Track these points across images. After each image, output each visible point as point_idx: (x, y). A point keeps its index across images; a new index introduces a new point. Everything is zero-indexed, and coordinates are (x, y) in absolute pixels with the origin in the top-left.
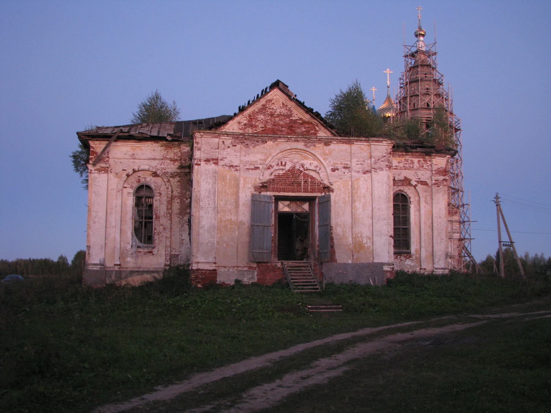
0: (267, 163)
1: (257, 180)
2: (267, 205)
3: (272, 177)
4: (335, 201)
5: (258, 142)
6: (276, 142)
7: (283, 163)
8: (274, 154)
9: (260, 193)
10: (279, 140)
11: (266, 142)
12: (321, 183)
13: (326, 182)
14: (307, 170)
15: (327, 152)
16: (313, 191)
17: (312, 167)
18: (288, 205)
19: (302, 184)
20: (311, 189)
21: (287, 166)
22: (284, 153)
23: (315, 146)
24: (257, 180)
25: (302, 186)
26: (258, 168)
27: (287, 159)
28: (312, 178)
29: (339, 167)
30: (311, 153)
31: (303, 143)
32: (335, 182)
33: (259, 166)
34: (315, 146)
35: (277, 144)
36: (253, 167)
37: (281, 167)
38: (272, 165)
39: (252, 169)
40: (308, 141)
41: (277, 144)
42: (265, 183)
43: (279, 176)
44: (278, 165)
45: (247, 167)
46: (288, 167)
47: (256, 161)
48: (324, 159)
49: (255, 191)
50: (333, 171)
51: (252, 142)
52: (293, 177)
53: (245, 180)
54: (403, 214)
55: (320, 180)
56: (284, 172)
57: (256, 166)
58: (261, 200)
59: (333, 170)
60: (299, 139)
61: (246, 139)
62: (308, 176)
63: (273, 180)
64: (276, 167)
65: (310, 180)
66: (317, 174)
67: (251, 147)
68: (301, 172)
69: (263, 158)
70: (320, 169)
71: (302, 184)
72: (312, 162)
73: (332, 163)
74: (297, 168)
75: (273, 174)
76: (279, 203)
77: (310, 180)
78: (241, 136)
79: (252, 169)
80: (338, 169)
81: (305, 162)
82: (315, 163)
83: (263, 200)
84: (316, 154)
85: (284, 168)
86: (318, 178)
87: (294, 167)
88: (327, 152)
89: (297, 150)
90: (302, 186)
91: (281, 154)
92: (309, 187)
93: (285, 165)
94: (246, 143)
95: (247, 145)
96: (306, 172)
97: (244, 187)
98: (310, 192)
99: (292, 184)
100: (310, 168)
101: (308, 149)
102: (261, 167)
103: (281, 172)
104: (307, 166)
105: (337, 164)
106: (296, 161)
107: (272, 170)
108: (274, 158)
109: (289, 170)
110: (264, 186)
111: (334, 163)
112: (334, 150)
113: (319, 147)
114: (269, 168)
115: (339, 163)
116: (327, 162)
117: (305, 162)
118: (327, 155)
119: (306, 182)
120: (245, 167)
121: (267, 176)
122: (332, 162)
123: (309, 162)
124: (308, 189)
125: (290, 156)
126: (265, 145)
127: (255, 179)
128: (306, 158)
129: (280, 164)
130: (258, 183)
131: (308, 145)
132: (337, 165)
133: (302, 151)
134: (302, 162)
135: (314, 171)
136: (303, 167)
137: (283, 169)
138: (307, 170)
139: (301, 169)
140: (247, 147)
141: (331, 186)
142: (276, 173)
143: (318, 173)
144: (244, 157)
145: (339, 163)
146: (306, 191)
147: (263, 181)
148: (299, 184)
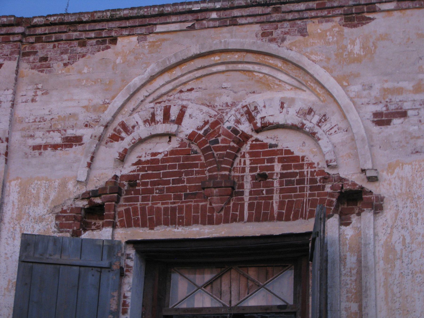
0: (107, 116)
1: (70, 186)
2: (91, 278)
3: (128, 169)
4: (390, 249)
5: (83, 44)
6: (151, 38)
7: (174, 113)
8: (137, 81)
9: (76, 234)
10: (159, 28)
11: (114, 41)
12: (326, 178)
13: (349, 173)
14: (266, 127)
15: (357, 49)
16: (289, 213)
17: (291, 117)
18: (210, 283)
19: (247, 187)
20: (281, 204)
21: (186, 121)
22: (177, 72)
23: (303, 32)
24: (70, 186)
25: (246, 197)
26: (77, 140)
27: (193, 95)
28: (289, 159)
29: (406, 106)
30: (285, 61)
31: (257, 28)
32: (391, 168)
33: (79, 132)
34: (303, 32)
35: (152, 45)
36: (57, 139)
37: (161, 128)
38: (130, 123)
39: (55, 147)
40: (276, 16)
41: (152, 45)
42: (96, 193)
43: (153, 164)
44: (152, 120)
45: (38, 141)
46: (189, 126)
47: (73, 116)
48: (339, 80)
49: (61, 227)
50: (379, 123)
51: (63, 46)
52: (213, 163)
53: (24, 191)
54: (332, 201)
55: (323, 165)
56: (175, 144)
57: (70, 133)
58: (65, 259)
59: (382, 120)
60: (236, 13)
61: (39, 39)
62: (271, 151)
63: (132, 180)
64: (143, 131)
65: (278, 168)
66: (309, 142)
67: (57, 66)
68: (246, 137)
69: (98, 100)
70: (324, 119)
71: (247, 187)
72: (289, 94)
73: (375, 92)
74: (229, 123)
75: (133, 158)
76: (290, 301)
77: (278, 168)
78: (19, 30)
79: (55, 147)
80: (403, 114)
81: (259, 99)
82: (305, 98)
83: (76, 260)
84: (305, 62)
85: (172, 128)
86: (315, 159)
87: (216, 123)
88: (357, 49)
89: (228, 57)
90: (246, 197)
91: (166, 77)
92: (276, 197)
93: (179, 120)
94: (41, 54)
95: (45, 59)
96: (263, 137)
97: (20, 218)
98: (280, 218)
99: (202, 190)
100: (280, 119)
101: (272, 48)
102: (87, 134)
103: (163, 148)
104: (271, 114)
105: (400, 91)
106: (226, 98)
107: (127, 141)
108: (140, 96)
109: (192, 137)
110: (93, 210)
111: (386, 91)
112: (384, 37)
113: (322, 36)
114: (116, 138)
115: (408, 85)
116: (355, 88)
117: (259, 99)
118: (358, 60)
119: (262, 178)
120: (31, 142)
121: (107, 169)
122: (377, 86)
123: (278, 96)
124: (268, 206)
125: (205, 82)
126: (109, 53)
127: (63, 184)
128: (267, 84)
129: (159, 117)
130: (72, 195)
131: (276, 34)
132: (396, 98)
133: (250, 57)
134: (249, 100)
135: (293, 128)
136: (251, 119)
137: (170, 136)
138: (266, 127)
139: (245, 127)
140: (41, 69)
141: (369, 186)
142: (143, 152)
143: (312, 135)
144: (30, 105)
145: (408, 85)
146: (260, 214)
147: (91, 187)
148: (233, 189)
